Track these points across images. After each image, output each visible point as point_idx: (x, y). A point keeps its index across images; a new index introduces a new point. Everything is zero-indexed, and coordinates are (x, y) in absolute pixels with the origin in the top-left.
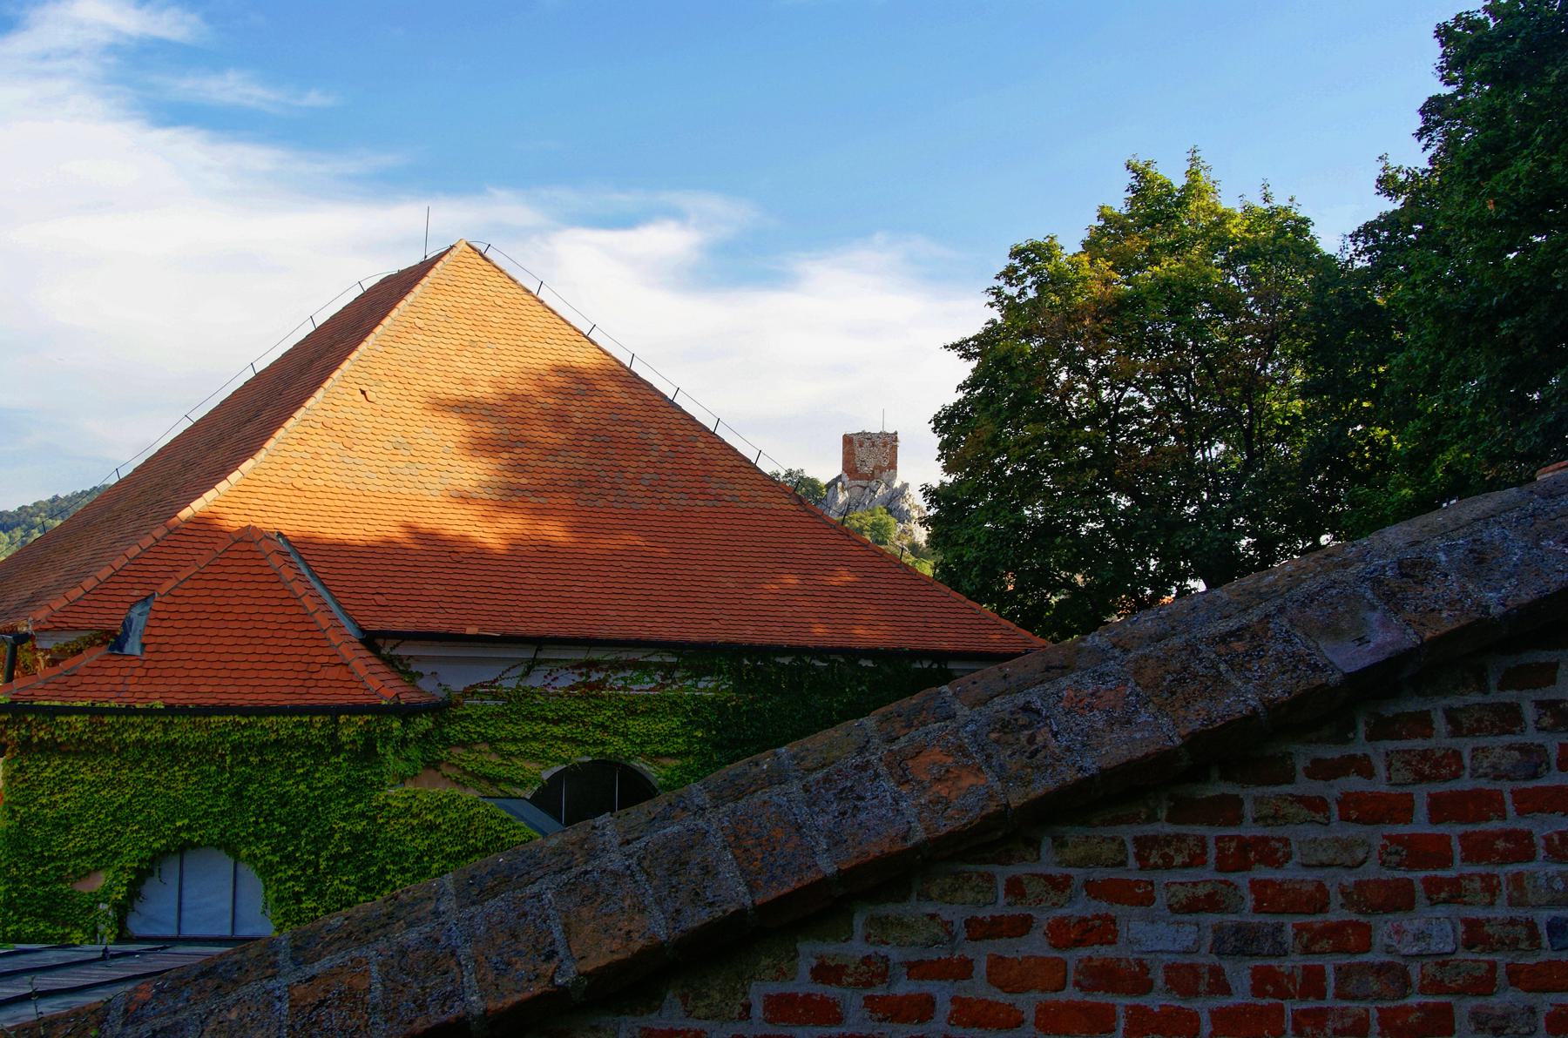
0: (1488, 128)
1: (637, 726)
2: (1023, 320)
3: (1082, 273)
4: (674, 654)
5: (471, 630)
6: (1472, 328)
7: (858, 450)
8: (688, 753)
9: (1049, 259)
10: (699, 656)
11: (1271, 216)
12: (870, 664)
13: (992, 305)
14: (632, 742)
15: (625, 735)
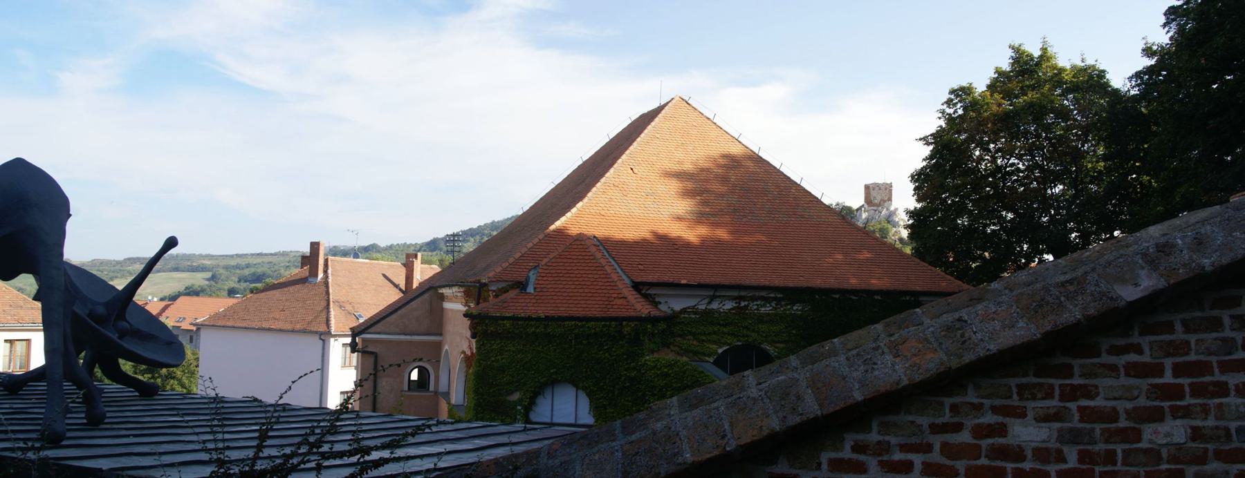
5: (683, 282)
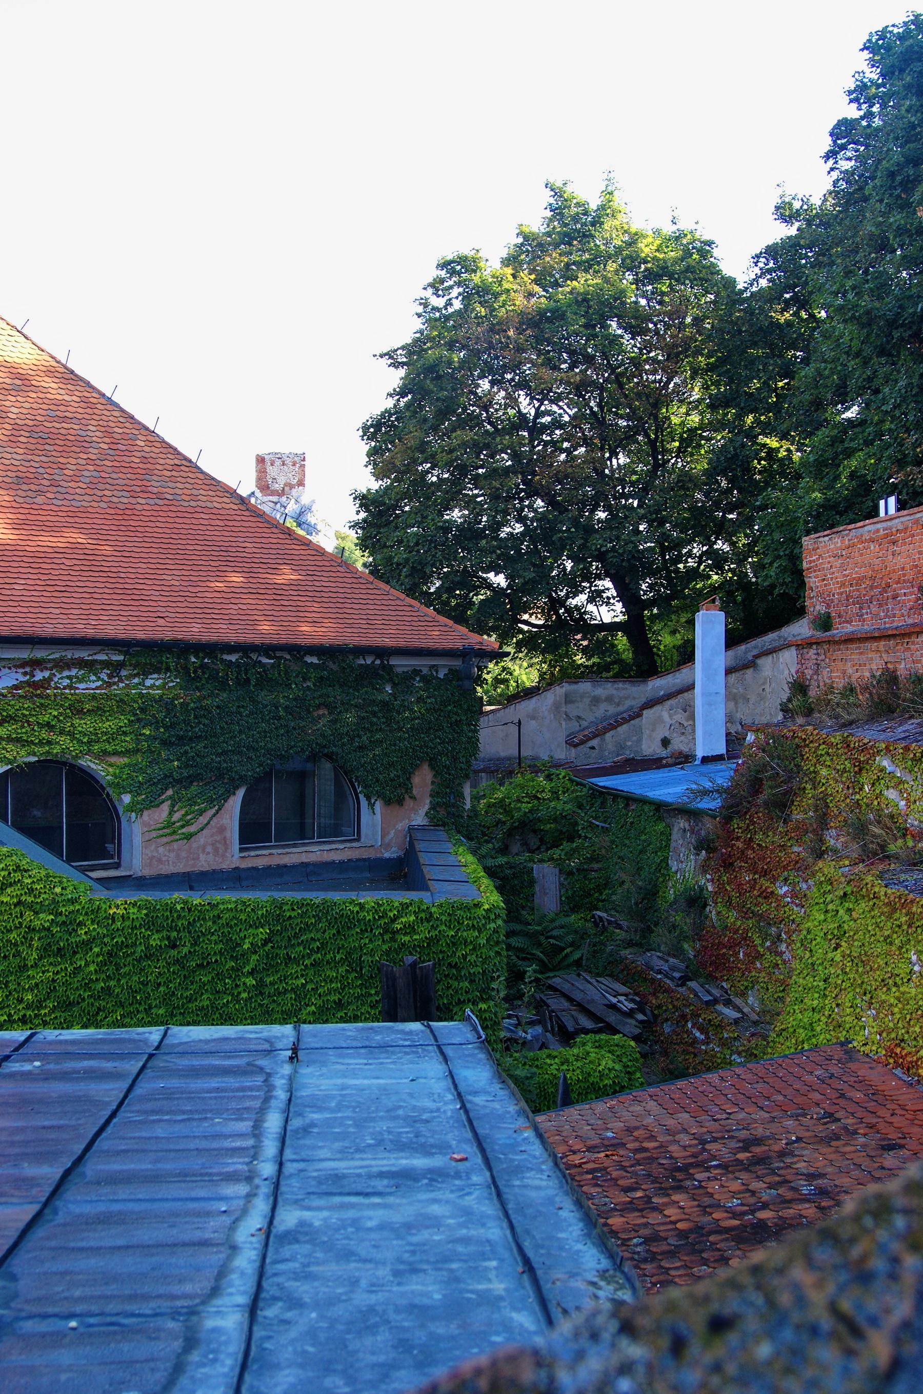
0: (907, 142)
1: (84, 724)
2: (449, 331)
3: (506, 285)
4: (120, 652)
6: (896, 334)
7: (269, 469)
8: (137, 751)
9: (475, 271)
10: (146, 654)
11: (677, 238)
12: (315, 660)
13: (419, 315)
14: (80, 742)
15: (71, 734)
